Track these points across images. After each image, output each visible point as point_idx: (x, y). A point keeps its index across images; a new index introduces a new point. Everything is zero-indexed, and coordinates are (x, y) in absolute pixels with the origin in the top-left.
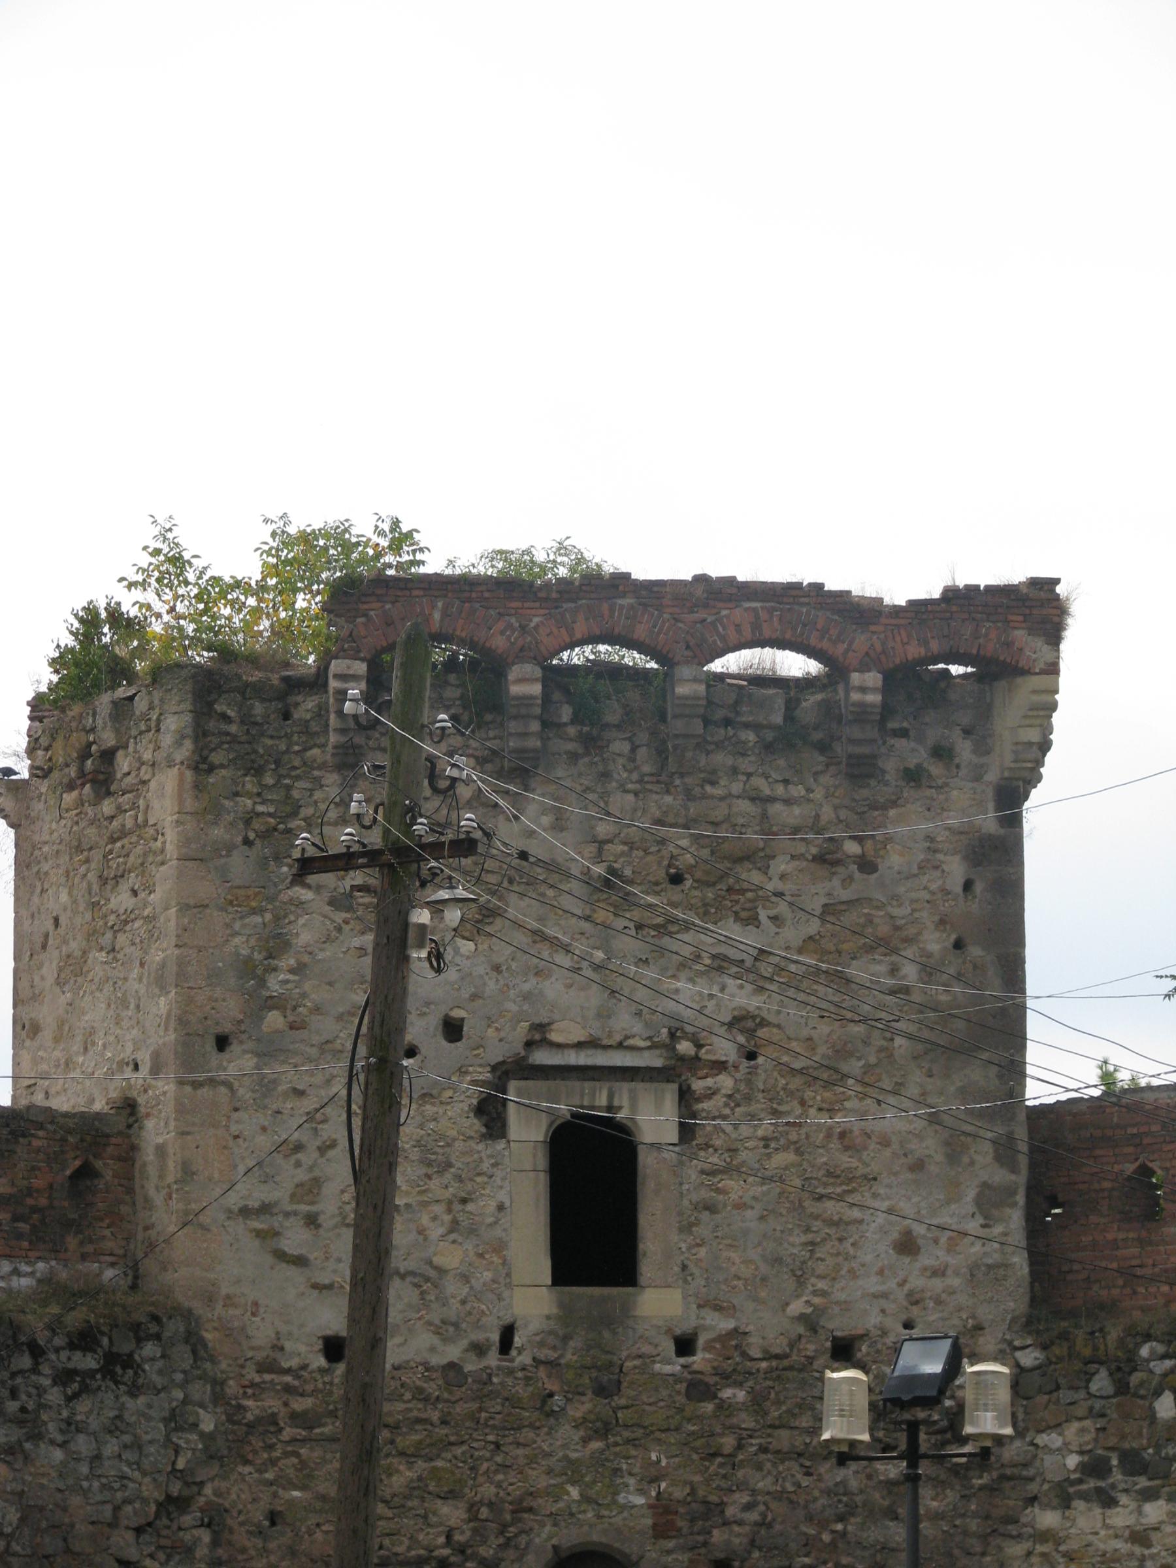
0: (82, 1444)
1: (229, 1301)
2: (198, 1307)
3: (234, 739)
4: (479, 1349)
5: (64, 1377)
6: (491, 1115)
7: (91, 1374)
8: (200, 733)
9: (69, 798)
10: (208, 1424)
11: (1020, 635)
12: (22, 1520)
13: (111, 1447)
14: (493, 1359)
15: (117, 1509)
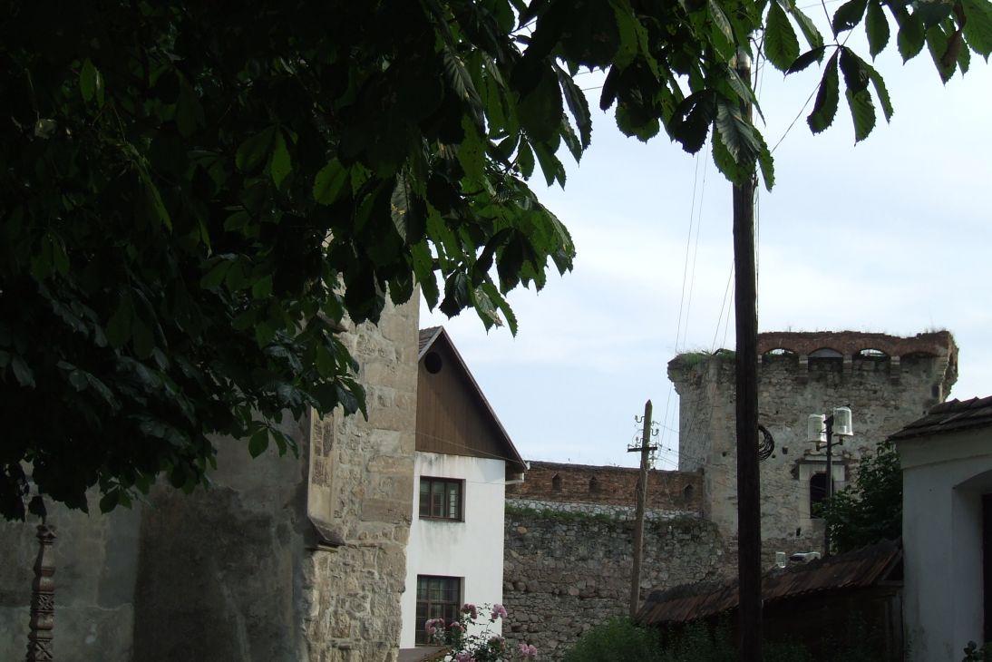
0: (686, 559)
1: (725, 522)
2: (718, 523)
3: (304, 350)
4: (791, 535)
5: (680, 541)
6: (795, 473)
7: (688, 540)
8: (719, 374)
9: (691, 388)
10: (720, 553)
11: (937, 346)
12: (669, 577)
13: (694, 558)
14: (795, 537)
15: (695, 575)
